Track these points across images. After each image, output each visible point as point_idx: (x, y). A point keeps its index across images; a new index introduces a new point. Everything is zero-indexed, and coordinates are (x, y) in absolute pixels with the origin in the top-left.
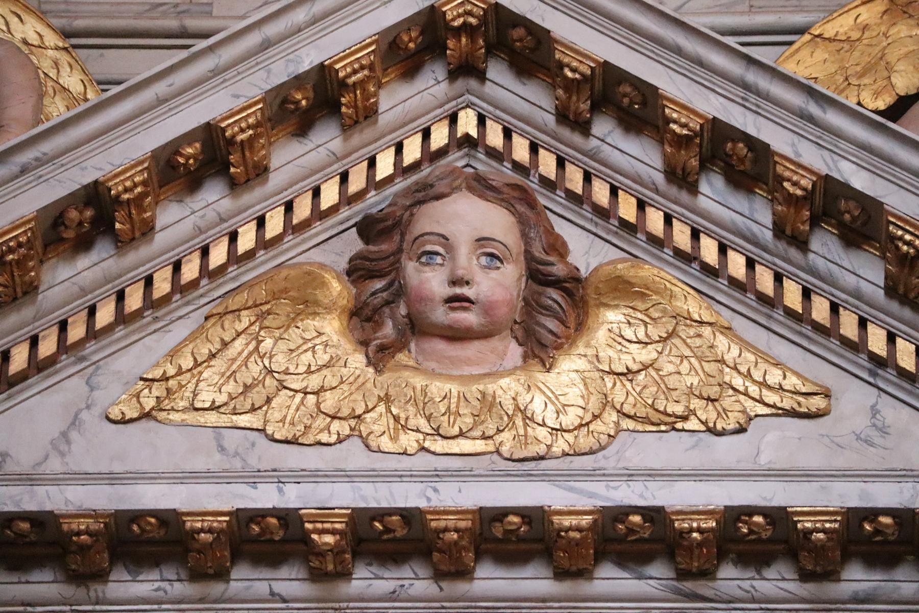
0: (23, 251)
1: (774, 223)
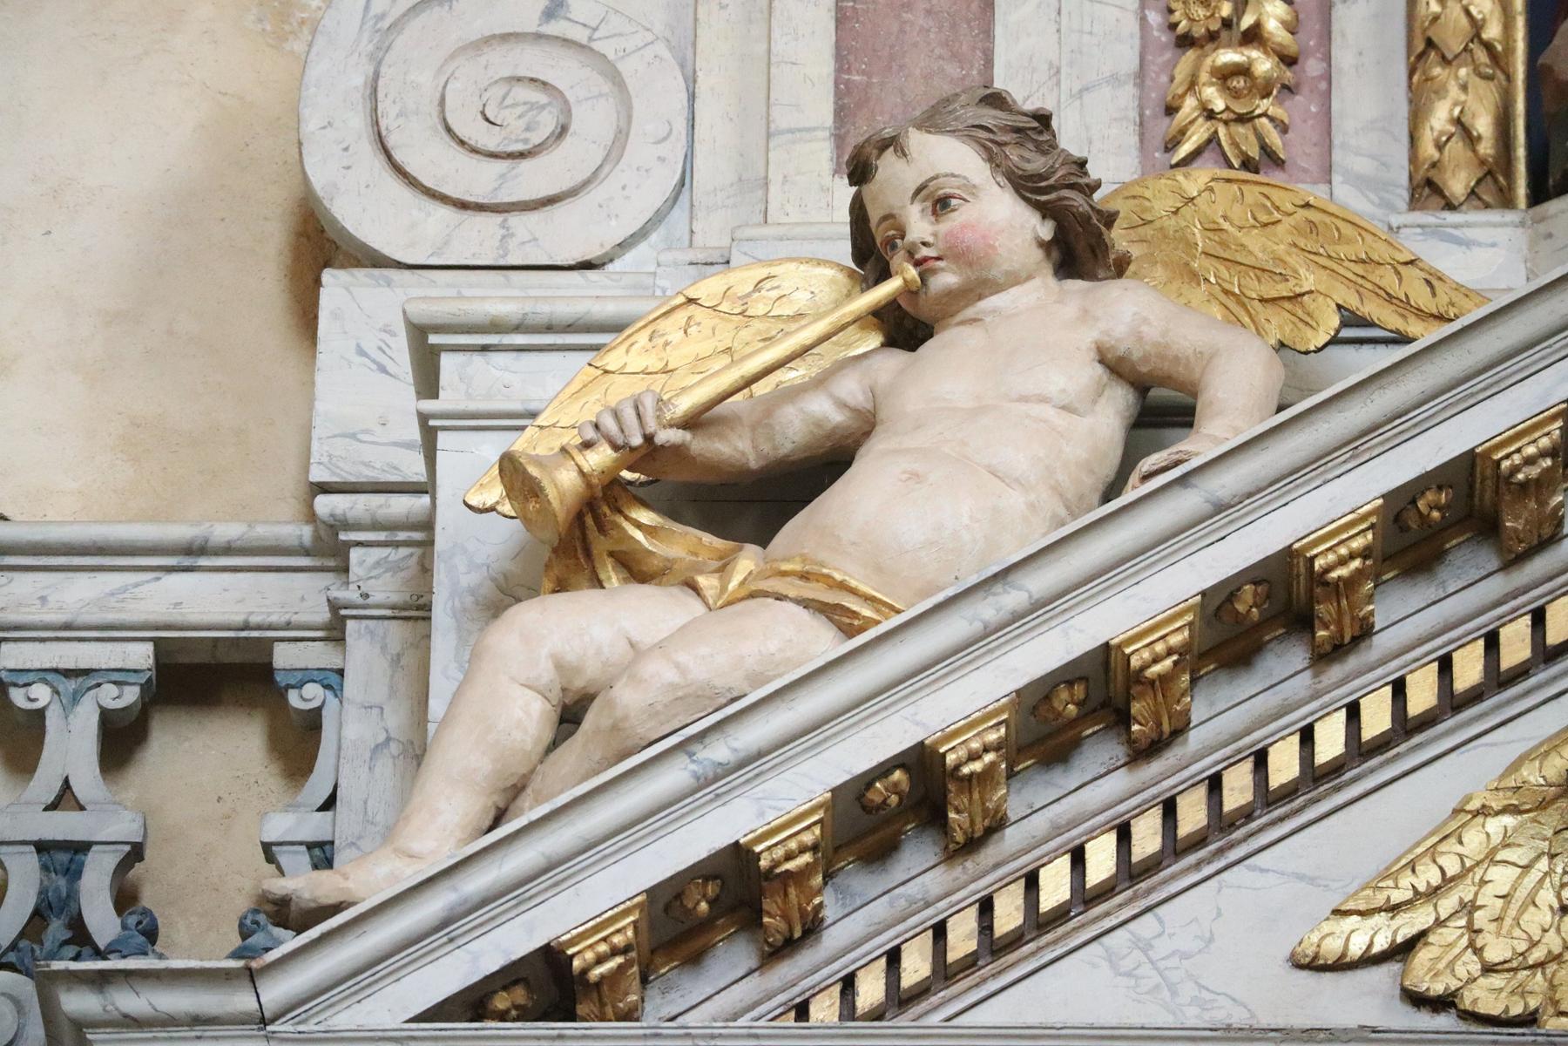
0: (1356, 563)
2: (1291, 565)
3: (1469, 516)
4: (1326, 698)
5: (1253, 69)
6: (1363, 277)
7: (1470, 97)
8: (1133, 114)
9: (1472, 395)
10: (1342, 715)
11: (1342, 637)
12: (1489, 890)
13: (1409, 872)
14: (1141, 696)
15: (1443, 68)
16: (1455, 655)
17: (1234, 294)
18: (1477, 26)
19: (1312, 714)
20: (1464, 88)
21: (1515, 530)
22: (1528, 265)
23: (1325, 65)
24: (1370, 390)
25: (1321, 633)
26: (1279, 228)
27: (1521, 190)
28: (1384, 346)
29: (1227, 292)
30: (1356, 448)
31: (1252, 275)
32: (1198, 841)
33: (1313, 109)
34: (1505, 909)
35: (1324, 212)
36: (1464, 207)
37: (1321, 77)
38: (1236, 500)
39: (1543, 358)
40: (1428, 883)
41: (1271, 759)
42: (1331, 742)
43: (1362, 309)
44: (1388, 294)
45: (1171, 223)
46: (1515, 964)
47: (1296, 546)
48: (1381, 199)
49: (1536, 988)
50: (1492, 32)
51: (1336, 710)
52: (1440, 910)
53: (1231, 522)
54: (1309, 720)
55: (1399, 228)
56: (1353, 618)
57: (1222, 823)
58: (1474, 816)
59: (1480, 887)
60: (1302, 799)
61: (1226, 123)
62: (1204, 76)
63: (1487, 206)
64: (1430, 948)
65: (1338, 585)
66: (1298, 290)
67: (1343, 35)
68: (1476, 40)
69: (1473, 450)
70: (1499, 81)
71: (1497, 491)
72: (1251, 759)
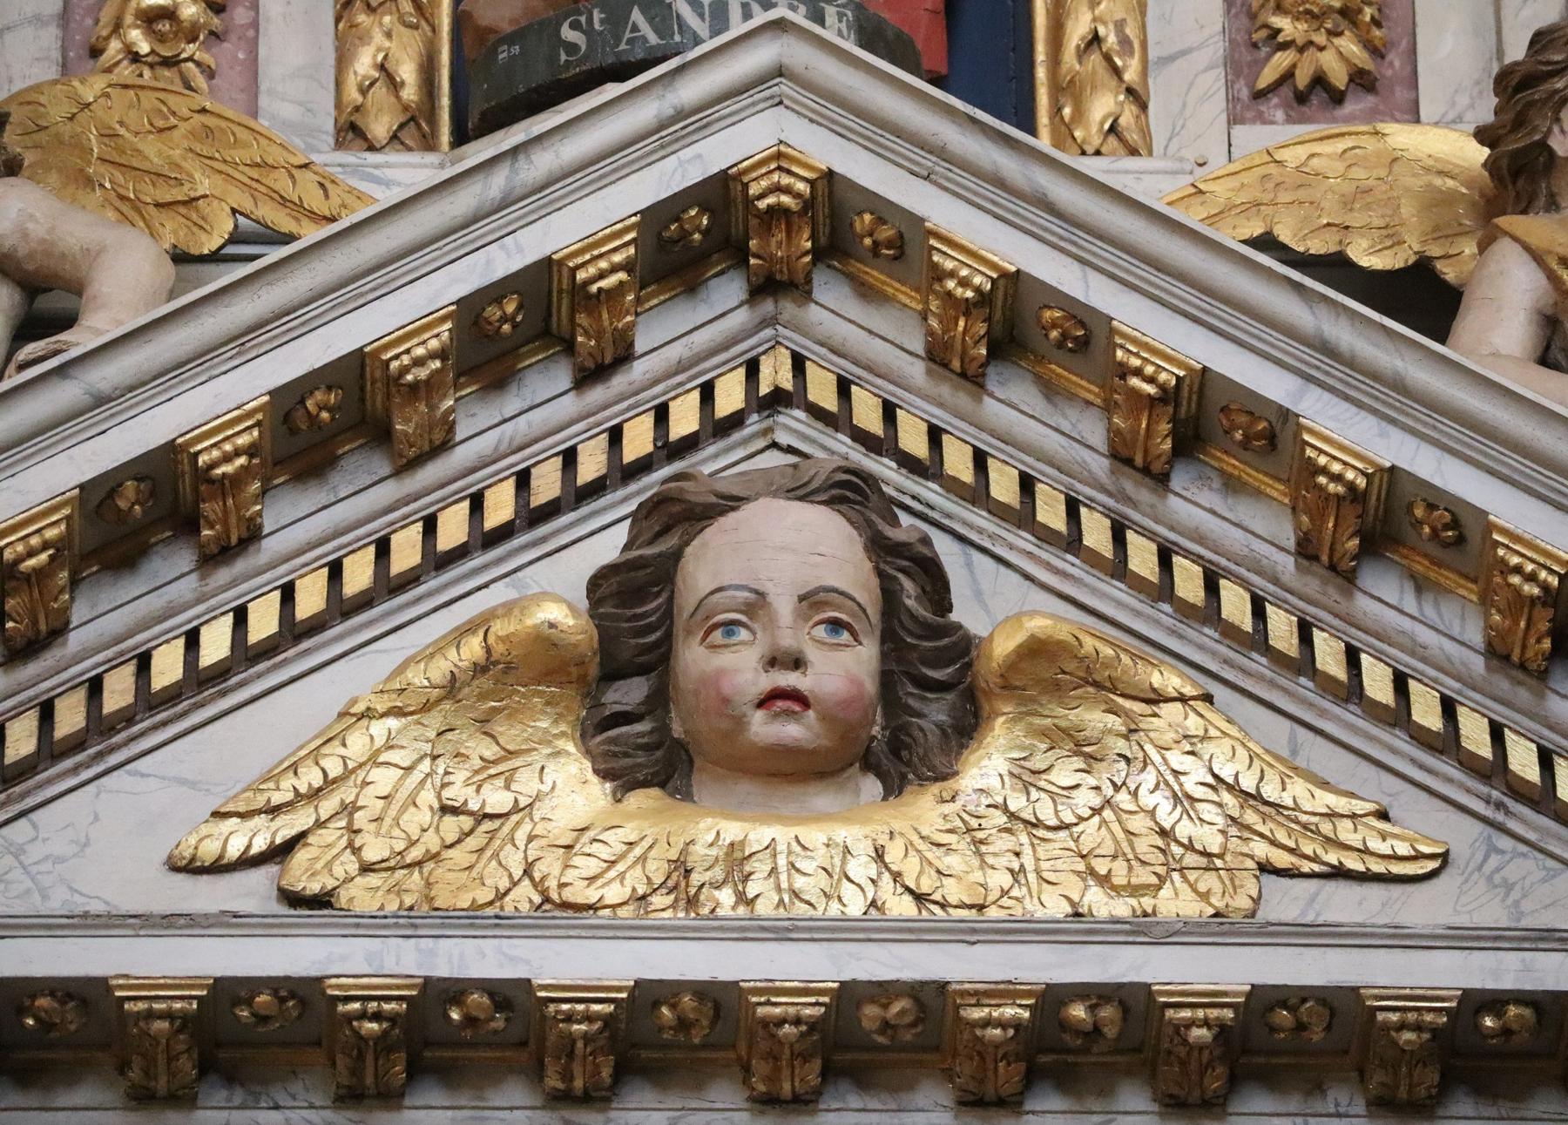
0: (242, 460)
1: (1299, 544)
2: (176, 462)
3: (363, 421)
4: (213, 602)
5: (179, 13)
6: (257, 181)
8: (56, 55)
9: (361, 295)
10: (229, 620)
11: (229, 538)
12: (369, 790)
13: (291, 774)
14: (16, 592)
16: (345, 561)
17: (128, 199)
19: (198, 617)
20: (389, 35)
21: (406, 434)
24: (257, 286)
25: (206, 532)
26: (176, 133)
29: (122, 198)
30: (243, 344)
31: (147, 180)
32: (77, 743)
33: (241, 56)
34: (385, 810)
36: (387, 149)
38: (118, 392)
40: (310, 784)
41: (154, 662)
42: (216, 645)
44: (281, 197)
45: (67, 129)
46: (392, 863)
47: (180, 441)
49: (412, 886)
51: (223, 614)
52: (321, 811)
53: (112, 416)
54: (195, 623)
56: (240, 518)
57: (101, 727)
58: (359, 719)
59: (362, 788)
60: (185, 703)
61: (151, 66)
62: (129, 19)
63: (410, 149)
64: (309, 848)
65: (224, 484)
66: (193, 194)
69: (361, 349)
71: (388, 396)
72: (134, 662)
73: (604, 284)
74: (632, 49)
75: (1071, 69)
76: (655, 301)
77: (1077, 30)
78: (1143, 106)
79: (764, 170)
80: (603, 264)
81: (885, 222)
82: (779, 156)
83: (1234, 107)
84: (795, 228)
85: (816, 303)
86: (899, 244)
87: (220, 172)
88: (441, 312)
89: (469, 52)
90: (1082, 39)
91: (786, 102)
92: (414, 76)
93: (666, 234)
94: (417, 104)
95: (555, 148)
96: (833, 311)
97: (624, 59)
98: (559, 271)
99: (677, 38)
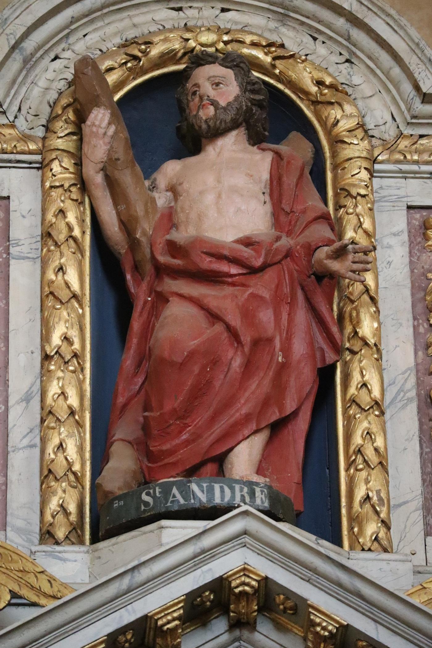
6: (21, 578)
7: (67, 495)
15: (56, 482)
18: (70, 465)
20: (64, 491)
22: (90, 570)
23: (4, 479)
27: (88, 542)
28: (28, 607)
35: (5, 548)
36: (63, 544)
37: (3, 484)
39: (97, 617)
43: (20, 592)
44: (31, 586)
48: (27, 538)
50: (76, 467)
55: (35, 552)
63: (73, 544)
67: (13, 466)
68: (69, 471)
70: (79, 489)
73: (169, 626)
74: (173, 506)
75: (357, 511)
76: (189, 630)
77: (360, 493)
78: (389, 528)
79: (238, 576)
80: (169, 618)
81: (289, 599)
82: (244, 569)
83: (427, 528)
84: (250, 600)
85: (258, 632)
86: (295, 609)
87: (4, 573)
88: (101, 640)
89: (100, 502)
90: (362, 498)
91: (248, 546)
92: (75, 510)
93: (195, 603)
94: (77, 523)
95: (150, 567)
96: (265, 636)
97: (169, 509)
98: (151, 621)
99: (192, 501)
